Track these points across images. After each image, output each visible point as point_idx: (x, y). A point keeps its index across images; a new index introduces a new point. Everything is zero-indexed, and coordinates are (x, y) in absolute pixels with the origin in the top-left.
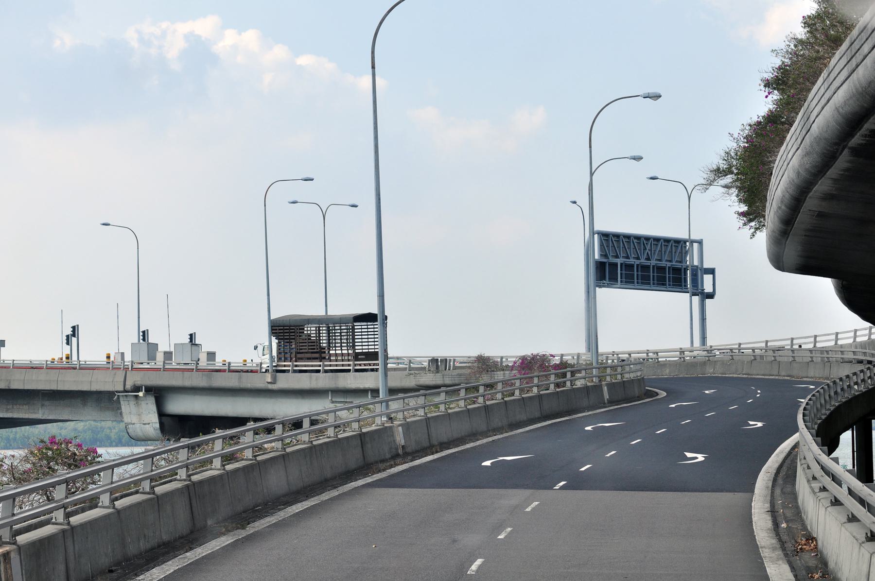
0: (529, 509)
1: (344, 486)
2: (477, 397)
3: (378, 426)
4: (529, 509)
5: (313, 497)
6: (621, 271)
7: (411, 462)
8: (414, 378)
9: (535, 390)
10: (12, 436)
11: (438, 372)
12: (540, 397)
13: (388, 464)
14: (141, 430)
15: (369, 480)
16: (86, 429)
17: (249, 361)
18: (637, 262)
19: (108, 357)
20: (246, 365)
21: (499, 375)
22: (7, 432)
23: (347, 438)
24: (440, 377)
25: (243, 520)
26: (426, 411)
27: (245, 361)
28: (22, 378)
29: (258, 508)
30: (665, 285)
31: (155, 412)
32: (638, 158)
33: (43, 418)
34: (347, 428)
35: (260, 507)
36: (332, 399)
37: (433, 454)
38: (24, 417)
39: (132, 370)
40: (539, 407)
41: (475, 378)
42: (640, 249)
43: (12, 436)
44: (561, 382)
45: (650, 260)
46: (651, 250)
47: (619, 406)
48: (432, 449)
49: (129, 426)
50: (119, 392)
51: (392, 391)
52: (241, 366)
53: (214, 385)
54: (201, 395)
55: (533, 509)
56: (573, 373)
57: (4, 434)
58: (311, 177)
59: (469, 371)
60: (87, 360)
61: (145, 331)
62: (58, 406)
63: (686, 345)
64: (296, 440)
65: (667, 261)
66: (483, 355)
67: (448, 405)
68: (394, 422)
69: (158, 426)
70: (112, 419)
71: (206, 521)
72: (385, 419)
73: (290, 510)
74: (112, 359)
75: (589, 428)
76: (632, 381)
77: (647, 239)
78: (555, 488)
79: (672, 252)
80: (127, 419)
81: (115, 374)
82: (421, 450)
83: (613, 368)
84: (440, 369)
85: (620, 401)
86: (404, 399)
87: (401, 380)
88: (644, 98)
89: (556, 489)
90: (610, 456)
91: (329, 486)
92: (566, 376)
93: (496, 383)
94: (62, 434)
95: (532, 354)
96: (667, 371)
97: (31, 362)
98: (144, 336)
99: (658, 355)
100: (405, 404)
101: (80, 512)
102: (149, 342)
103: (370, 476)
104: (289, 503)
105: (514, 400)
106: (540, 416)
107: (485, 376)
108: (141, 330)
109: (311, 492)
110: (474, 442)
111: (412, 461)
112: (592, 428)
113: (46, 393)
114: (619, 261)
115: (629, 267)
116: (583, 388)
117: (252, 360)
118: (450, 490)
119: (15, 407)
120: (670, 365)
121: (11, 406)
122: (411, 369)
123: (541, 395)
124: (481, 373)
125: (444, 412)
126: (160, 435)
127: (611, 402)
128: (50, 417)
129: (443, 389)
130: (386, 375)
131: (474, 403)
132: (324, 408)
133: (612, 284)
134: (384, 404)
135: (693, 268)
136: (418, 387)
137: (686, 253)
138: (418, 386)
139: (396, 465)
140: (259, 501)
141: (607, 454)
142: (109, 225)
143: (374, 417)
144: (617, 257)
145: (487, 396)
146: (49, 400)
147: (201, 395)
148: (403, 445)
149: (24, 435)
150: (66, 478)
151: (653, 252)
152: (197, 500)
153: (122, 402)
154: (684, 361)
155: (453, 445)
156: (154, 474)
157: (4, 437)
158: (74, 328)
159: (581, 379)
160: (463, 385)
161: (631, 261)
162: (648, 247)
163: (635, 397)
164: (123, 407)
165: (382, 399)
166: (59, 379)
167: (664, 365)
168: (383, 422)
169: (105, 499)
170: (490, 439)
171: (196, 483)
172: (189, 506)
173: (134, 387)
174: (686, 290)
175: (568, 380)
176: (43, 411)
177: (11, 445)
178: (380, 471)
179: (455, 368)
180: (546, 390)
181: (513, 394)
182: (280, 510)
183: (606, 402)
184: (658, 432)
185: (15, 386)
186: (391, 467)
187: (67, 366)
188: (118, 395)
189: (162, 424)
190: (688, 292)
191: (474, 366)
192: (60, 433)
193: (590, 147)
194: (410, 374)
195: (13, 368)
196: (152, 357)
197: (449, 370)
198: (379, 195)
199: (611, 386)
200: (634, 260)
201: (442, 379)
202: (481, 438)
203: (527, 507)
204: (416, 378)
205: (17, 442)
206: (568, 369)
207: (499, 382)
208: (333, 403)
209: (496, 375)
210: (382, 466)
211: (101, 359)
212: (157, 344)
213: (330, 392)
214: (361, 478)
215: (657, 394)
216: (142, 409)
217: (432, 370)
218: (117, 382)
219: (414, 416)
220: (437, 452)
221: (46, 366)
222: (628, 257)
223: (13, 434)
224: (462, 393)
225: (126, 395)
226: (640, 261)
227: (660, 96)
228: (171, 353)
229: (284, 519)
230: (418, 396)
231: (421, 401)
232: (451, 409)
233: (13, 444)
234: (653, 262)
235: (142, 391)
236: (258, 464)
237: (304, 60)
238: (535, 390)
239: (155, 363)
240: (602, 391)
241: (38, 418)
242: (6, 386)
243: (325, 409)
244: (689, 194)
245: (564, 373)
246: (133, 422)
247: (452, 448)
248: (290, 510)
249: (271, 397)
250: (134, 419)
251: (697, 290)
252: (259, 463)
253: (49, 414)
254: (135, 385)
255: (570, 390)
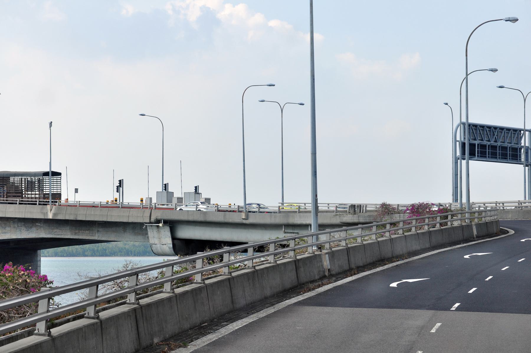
0: (433, 331)
1: (280, 303)
2: (384, 232)
3: (309, 254)
4: (433, 331)
5: (252, 314)
6: (478, 149)
7: (335, 282)
8: (339, 217)
9: (426, 228)
10: (96, 249)
11: (355, 214)
12: (430, 233)
13: (317, 284)
14: (161, 249)
15: (300, 298)
16: (141, 245)
17: (232, 204)
18: (489, 143)
19: (142, 200)
20: (231, 207)
21: (396, 217)
22: (93, 246)
23: (284, 264)
24: (356, 217)
25: (187, 337)
26: (347, 242)
27: (230, 204)
28: (85, 213)
29: (204, 325)
30: (507, 159)
31: (169, 237)
32: (495, 70)
33: (98, 239)
34: (286, 254)
35: (206, 324)
36: (284, 231)
37: (352, 276)
38: (86, 238)
39: (155, 209)
40: (429, 240)
41: (380, 218)
42: (490, 135)
43: (96, 249)
44: (443, 223)
45: (497, 142)
46: (498, 136)
47: (482, 241)
48: (351, 272)
49: (153, 246)
50: (147, 223)
51: (322, 227)
52: (226, 208)
53: (208, 220)
54: (200, 226)
55: (437, 330)
56: (453, 216)
57: (91, 247)
58: (273, 83)
59: (376, 213)
60: (130, 202)
61: (166, 184)
62: (108, 231)
63: (522, 199)
64: (244, 265)
65: (508, 143)
66: (386, 203)
67: (363, 238)
68: (322, 251)
69: (171, 246)
70: (142, 241)
71: (152, 339)
72: (316, 248)
73: (231, 327)
74: (144, 202)
75: (467, 257)
76: (492, 223)
77: (495, 128)
78: (451, 309)
79: (511, 137)
80: (152, 241)
81: (144, 211)
82: (342, 272)
83: (480, 212)
84: (357, 212)
85: (484, 236)
86: (330, 233)
87: (330, 219)
88: (506, 21)
89: (453, 310)
90: (489, 280)
91: (268, 304)
92: (448, 218)
93: (398, 222)
94: (126, 248)
95: (419, 203)
96: (510, 216)
97: (94, 203)
98: (165, 187)
99: (503, 205)
100: (331, 237)
101: (25, 336)
102: (169, 191)
103: (301, 294)
104: (231, 319)
105: (411, 235)
106: (430, 247)
107: (387, 217)
108: (164, 184)
109: (252, 309)
110: (382, 266)
111: (335, 281)
112: (469, 257)
113: (101, 223)
114: (476, 142)
115: (483, 147)
116: (459, 226)
117: (234, 204)
118: (366, 309)
119: (80, 232)
120: (512, 211)
121: (78, 231)
122: (337, 211)
123: (431, 231)
124: (384, 215)
125: (360, 243)
126: (173, 252)
127: (479, 237)
128: (103, 239)
129: (360, 226)
130: (317, 215)
131: (382, 236)
132: (269, 240)
133: (471, 158)
134: (315, 237)
135: (526, 148)
136: (342, 224)
137: (521, 138)
138: (342, 223)
139: (323, 285)
140: (205, 319)
141: (486, 279)
142: (145, 115)
143: (307, 247)
144: (475, 139)
145: (391, 232)
146: (102, 228)
147: (200, 226)
148: (329, 269)
149: (103, 248)
150: (136, 272)
151: (499, 136)
152: (144, 322)
153: (148, 230)
154: (522, 209)
155: (367, 268)
156: (139, 288)
157: (91, 249)
158: (120, 181)
159: (457, 220)
160: (374, 223)
161: (485, 142)
162: (496, 134)
163: (494, 234)
164: (149, 233)
165: (313, 233)
166: (108, 214)
167: (508, 212)
168: (313, 251)
169: (41, 327)
170: (395, 264)
171: (144, 306)
172: (136, 328)
173: (156, 220)
174: (520, 163)
175: (449, 221)
176: (98, 235)
177: (95, 254)
178: (310, 290)
179: (366, 211)
180: (433, 228)
181: (410, 230)
182: (223, 326)
183: (475, 237)
184: (520, 261)
185: (80, 218)
186: (319, 286)
187: (114, 206)
188: (146, 226)
189: (174, 245)
190: (523, 164)
191: (379, 210)
192: (125, 247)
193: (466, 56)
194: (337, 215)
195: (79, 206)
196: (169, 201)
197: (363, 212)
198: (314, 76)
199: (478, 225)
200: (486, 142)
201: (358, 219)
202: (387, 263)
203: (432, 328)
204: (340, 217)
205: (99, 252)
206: (449, 213)
207: (401, 221)
208: (285, 233)
209: (394, 217)
210: (311, 286)
211: (137, 202)
212: (173, 193)
213: (283, 226)
214: (295, 296)
215: (508, 232)
216: (161, 235)
217: (351, 212)
218: (145, 216)
219: (338, 245)
220: (355, 274)
221: (100, 205)
222: (482, 140)
223: (97, 247)
224: (374, 229)
225: (151, 225)
226: (491, 143)
227: (518, 20)
228: (182, 198)
229: (223, 337)
230: (341, 231)
231: (343, 234)
232: (365, 240)
233: (96, 253)
234: (499, 144)
235: (161, 223)
236: (205, 287)
237: (273, 23)
238: (426, 228)
239: (172, 205)
240: (472, 229)
241: (95, 239)
242: (74, 218)
243: (270, 240)
244: (525, 98)
245: (445, 216)
246: (155, 243)
247: (366, 271)
248: (231, 327)
249: (245, 228)
250: (156, 241)
251: (528, 162)
252: (207, 286)
253: (102, 237)
254: (157, 219)
255: (451, 228)
